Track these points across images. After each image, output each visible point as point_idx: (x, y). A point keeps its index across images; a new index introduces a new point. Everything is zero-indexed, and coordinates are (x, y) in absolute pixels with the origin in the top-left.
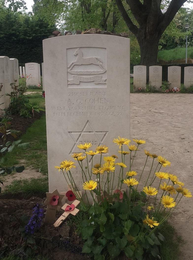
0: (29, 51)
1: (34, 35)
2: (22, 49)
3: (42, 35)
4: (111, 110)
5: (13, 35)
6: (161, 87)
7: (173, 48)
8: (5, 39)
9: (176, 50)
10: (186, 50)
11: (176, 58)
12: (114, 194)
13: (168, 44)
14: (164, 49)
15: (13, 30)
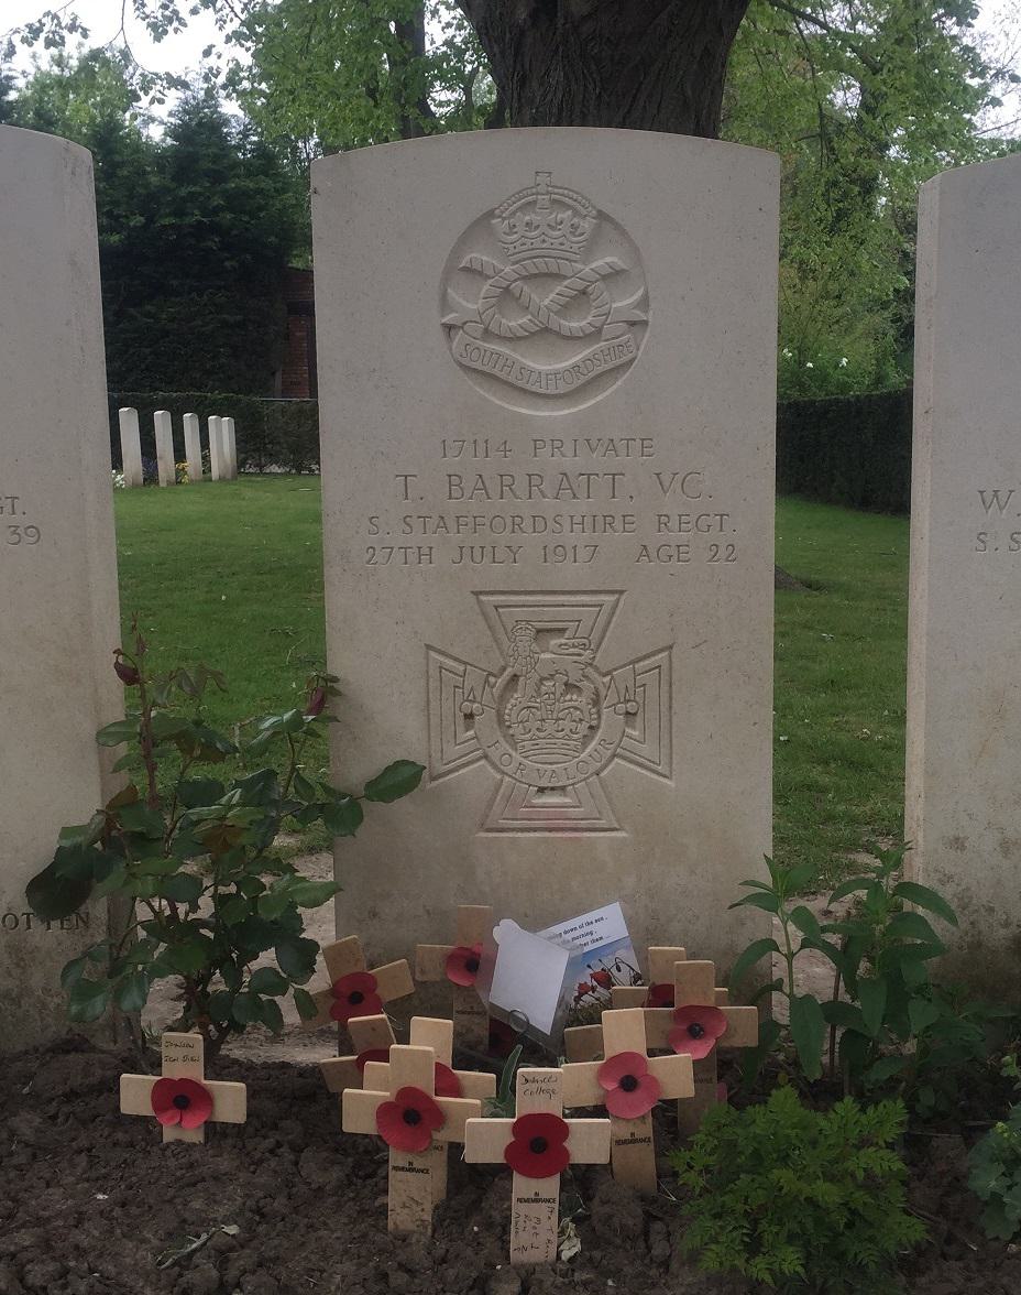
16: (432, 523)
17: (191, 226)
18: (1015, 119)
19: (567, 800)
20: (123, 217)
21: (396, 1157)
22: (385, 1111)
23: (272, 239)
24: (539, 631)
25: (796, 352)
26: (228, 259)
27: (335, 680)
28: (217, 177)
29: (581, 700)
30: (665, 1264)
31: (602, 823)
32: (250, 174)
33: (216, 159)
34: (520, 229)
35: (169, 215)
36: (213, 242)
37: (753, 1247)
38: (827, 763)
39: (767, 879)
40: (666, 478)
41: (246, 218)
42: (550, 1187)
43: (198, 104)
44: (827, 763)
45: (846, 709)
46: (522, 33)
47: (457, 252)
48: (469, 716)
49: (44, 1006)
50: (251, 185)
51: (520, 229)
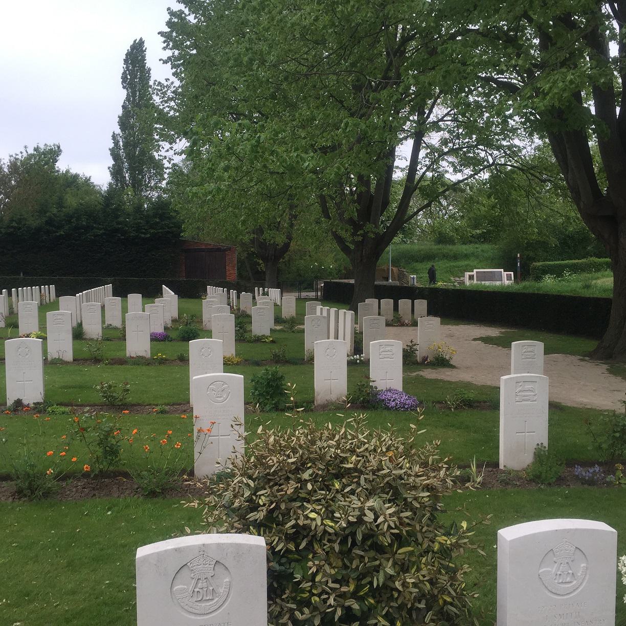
1: (152, 231)
3: (165, 230)
8: (104, 237)
11: (169, 53)
12: (271, 579)
15: (118, 223)
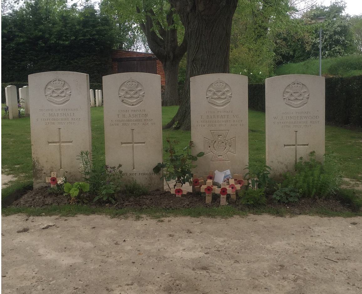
0: (66, 64)
2: (54, 61)
4: (79, 205)
5: (41, 38)
6: (157, 169)
7: (304, 60)
9: (308, 63)
10: (320, 63)
13: (297, 54)
14: (291, 62)
16: (205, 122)
17: (87, 39)
18: (304, 8)
19: (222, 157)
20: (69, 37)
21: (207, 195)
22: (206, 189)
23: (109, 42)
24: (218, 135)
25: (248, 70)
26: (97, 47)
27: (193, 142)
28: (94, 26)
29: (224, 144)
30: (238, 205)
31: (226, 160)
32: (103, 25)
33: (94, 21)
34: (216, 86)
35: (81, 36)
36: (93, 43)
37: (248, 202)
38: (256, 162)
39: (248, 165)
40: (234, 116)
41: (102, 37)
42: (225, 196)
43: (88, 7)
44: (256, 162)
45: (260, 154)
46: (188, 14)
47: (208, 89)
48: (209, 146)
49: (154, 185)
50: (103, 28)
51: (216, 86)
